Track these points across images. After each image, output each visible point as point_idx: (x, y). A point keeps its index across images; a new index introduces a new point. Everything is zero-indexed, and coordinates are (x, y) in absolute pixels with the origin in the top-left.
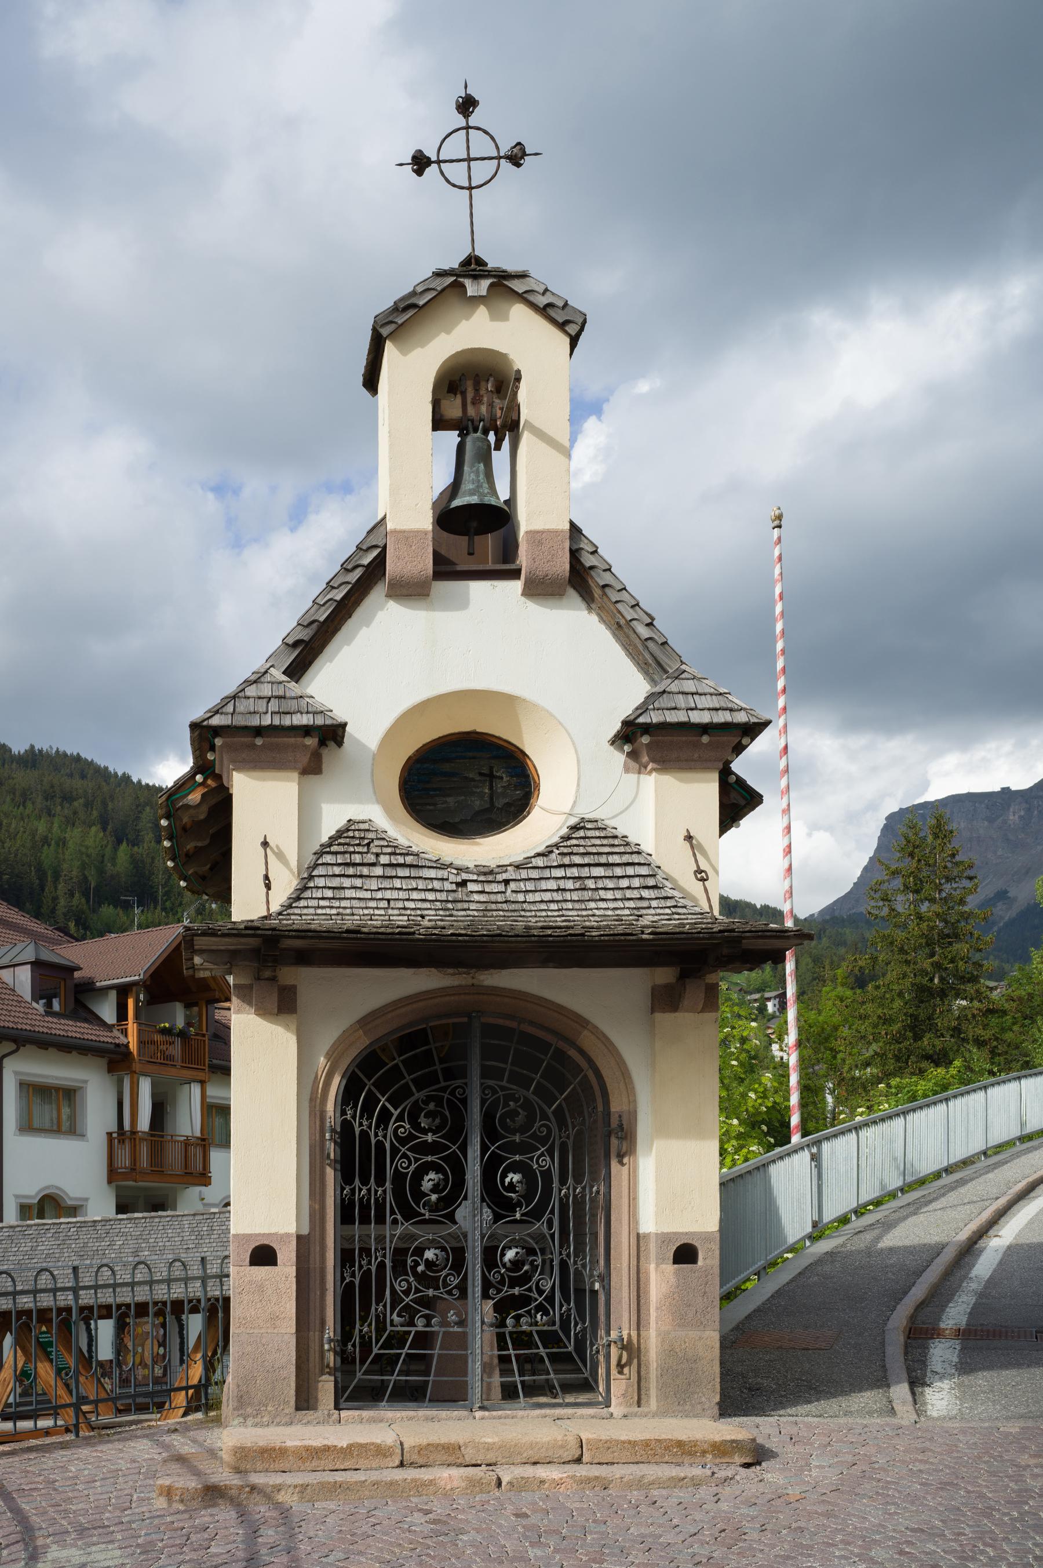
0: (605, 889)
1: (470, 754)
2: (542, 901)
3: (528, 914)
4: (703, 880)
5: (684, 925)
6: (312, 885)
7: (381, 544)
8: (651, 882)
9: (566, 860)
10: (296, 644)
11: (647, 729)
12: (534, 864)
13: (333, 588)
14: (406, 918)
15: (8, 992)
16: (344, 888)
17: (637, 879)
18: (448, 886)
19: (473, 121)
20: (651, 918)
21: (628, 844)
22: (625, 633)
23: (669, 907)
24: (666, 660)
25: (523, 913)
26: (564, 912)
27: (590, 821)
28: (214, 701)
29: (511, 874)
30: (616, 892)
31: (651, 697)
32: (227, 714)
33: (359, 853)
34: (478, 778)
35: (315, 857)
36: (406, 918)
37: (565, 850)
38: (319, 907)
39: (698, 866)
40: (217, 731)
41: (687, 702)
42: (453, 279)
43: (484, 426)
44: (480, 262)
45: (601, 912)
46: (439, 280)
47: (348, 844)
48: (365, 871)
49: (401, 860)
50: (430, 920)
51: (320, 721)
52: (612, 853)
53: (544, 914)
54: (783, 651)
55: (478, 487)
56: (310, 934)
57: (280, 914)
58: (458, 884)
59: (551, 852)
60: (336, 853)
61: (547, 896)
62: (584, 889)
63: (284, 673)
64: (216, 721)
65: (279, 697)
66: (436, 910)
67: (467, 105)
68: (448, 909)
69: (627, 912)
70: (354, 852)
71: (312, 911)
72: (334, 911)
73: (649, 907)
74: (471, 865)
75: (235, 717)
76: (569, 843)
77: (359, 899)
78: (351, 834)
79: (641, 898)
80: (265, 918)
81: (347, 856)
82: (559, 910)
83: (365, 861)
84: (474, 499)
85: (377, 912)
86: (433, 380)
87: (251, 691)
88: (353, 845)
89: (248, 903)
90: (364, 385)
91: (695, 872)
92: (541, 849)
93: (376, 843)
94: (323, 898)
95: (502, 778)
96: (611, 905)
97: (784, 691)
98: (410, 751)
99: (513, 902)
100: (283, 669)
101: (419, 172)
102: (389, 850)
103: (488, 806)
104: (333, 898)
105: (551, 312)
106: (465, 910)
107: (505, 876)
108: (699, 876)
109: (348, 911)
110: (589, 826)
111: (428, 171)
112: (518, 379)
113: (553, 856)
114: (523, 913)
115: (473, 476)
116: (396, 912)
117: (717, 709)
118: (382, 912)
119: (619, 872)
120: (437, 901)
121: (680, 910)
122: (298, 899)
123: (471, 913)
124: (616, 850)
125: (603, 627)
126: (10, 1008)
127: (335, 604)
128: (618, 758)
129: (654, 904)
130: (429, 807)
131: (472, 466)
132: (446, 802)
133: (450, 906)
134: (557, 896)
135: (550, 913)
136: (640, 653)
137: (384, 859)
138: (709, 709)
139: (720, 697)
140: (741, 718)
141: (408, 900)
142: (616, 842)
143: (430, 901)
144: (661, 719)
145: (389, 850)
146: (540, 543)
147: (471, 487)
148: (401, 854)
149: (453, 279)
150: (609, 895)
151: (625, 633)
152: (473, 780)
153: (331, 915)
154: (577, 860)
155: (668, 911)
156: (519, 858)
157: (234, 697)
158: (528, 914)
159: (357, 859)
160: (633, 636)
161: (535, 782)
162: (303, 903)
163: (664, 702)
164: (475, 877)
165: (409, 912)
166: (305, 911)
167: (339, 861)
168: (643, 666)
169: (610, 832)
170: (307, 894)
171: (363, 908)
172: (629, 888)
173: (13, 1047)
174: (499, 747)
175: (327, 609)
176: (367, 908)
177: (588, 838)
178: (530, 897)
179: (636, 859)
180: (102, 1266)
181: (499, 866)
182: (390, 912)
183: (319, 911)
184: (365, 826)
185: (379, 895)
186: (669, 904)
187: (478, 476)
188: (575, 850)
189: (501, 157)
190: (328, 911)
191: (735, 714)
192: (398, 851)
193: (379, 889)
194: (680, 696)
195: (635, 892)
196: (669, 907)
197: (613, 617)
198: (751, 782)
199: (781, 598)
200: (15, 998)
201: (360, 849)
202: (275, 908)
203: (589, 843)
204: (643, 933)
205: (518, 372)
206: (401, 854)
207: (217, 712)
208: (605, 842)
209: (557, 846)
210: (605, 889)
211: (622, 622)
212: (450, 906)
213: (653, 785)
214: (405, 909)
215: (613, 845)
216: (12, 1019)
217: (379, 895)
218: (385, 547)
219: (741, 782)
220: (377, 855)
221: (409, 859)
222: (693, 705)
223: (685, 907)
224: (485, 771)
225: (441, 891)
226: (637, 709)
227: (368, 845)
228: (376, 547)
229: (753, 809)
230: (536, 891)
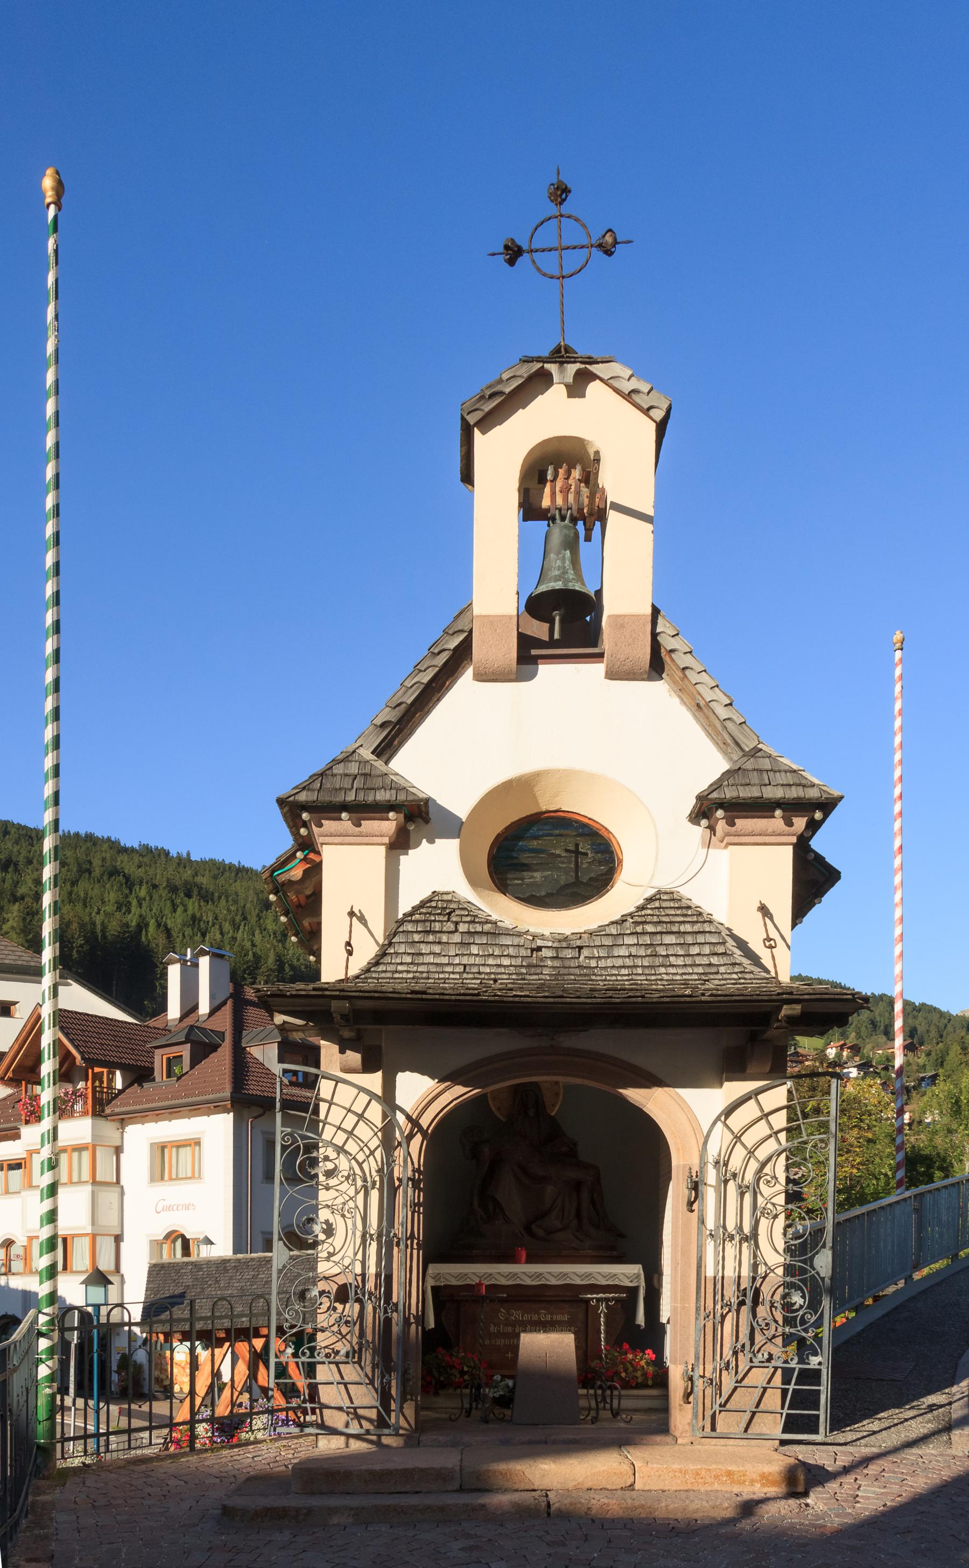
0: (676, 955)
1: (557, 832)
2: (613, 967)
3: (598, 978)
4: (771, 947)
5: (747, 988)
6: (392, 951)
7: (467, 628)
8: (721, 949)
9: (639, 929)
10: (383, 725)
11: (721, 805)
12: (608, 932)
13: (421, 671)
14: (479, 981)
15: (258, 1066)
16: (422, 954)
17: (707, 946)
18: (523, 952)
19: (566, 208)
20: (716, 982)
21: (700, 914)
22: (704, 714)
23: (736, 973)
24: (744, 740)
25: (594, 977)
26: (634, 977)
27: (666, 893)
28: (303, 777)
29: (585, 941)
30: (686, 958)
31: (727, 774)
32: (313, 790)
33: (439, 921)
34: (564, 854)
35: (395, 925)
36: (479, 981)
37: (639, 920)
38: (396, 972)
39: (768, 935)
40: (305, 807)
41: (762, 779)
42: (540, 365)
43: (571, 515)
44: (568, 349)
45: (670, 977)
46: (526, 366)
47: (430, 914)
48: (444, 938)
49: (479, 928)
50: (501, 984)
51: (402, 797)
52: (684, 922)
53: (614, 978)
54: (901, 762)
55: (563, 573)
56: (376, 995)
57: (357, 977)
58: (532, 950)
59: (626, 920)
60: (417, 921)
61: (619, 962)
62: (655, 955)
63: (373, 753)
64: (303, 797)
65: (365, 775)
66: (510, 974)
67: (560, 193)
68: (522, 974)
69: (696, 977)
70: (435, 921)
71: (389, 975)
72: (411, 975)
73: (717, 973)
74: (547, 933)
75: (321, 793)
76: (643, 913)
77: (437, 964)
78: (434, 904)
79: (710, 965)
80: (342, 980)
81: (428, 924)
82: (628, 975)
83: (445, 929)
84: (559, 585)
85: (452, 976)
86: (519, 468)
87: (339, 769)
88: (435, 914)
89: (333, 968)
90: (462, 481)
91: (764, 940)
92: (617, 917)
93: (457, 912)
94: (401, 964)
95: (586, 854)
96: (680, 971)
97: (901, 797)
98: (499, 828)
99: (585, 967)
100: (372, 749)
101: (511, 262)
102: (468, 919)
103: (573, 880)
104: (412, 963)
105: (635, 397)
106: (538, 974)
107: (579, 943)
108: (767, 944)
109: (425, 975)
110: (665, 897)
111: (520, 260)
112: (597, 460)
113: (627, 924)
114: (594, 977)
115: (559, 563)
116: (471, 976)
117: (790, 785)
118: (458, 976)
119: (689, 939)
120: (511, 966)
121: (747, 976)
122: (377, 964)
123: (543, 977)
124: (689, 919)
125: (684, 709)
126: (258, 1079)
127: (423, 686)
128: (698, 832)
129: (722, 969)
130: (516, 882)
131: (558, 553)
132: (532, 877)
133: (524, 971)
134: (628, 962)
135: (619, 978)
136: (718, 733)
137: (462, 928)
138: (782, 785)
139: (794, 774)
140: (813, 794)
141: (484, 965)
142: (690, 912)
143: (505, 966)
144: (735, 794)
145: (468, 919)
146: (622, 626)
147: (557, 573)
148: (479, 923)
149: (540, 365)
150: (680, 961)
151: (704, 714)
152: (559, 856)
153: (407, 979)
154: (650, 928)
155: (735, 976)
156: (593, 926)
157: (322, 774)
158: (598, 978)
159: (437, 926)
160: (712, 717)
161: (618, 859)
162: (381, 968)
163: (740, 779)
164: (550, 944)
165: (483, 976)
166: (383, 975)
167: (419, 929)
168: (722, 745)
169: (684, 903)
170: (387, 959)
171: (439, 973)
172: (698, 955)
173: (260, 1111)
174: (584, 826)
175: (415, 691)
176: (443, 972)
177: (663, 908)
178: (602, 963)
179: (707, 927)
180: (220, 1299)
181: (573, 934)
182: (465, 975)
183: (397, 975)
184: (449, 897)
185: (457, 961)
186: (736, 970)
187: (564, 562)
188: (649, 919)
189: (592, 246)
190: (405, 975)
191: (807, 790)
192: (477, 920)
193: (457, 955)
194: (755, 773)
195: (705, 958)
196: (736, 973)
197: (693, 699)
198: (830, 860)
199: (900, 714)
200: (264, 1071)
201: (441, 918)
202: (354, 971)
203: (667, 913)
204: (703, 995)
205: (597, 453)
206: (479, 923)
207: (304, 788)
208: (679, 912)
209: (631, 915)
210: (676, 955)
211: (702, 703)
212: (524, 971)
213: (724, 858)
214: (479, 973)
215: (686, 915)
216: (259, 1088)
217: (457, 961)
218: (471, 632)
219: (819, 859)
220: (457, 923)
221: (487, 927)
222: (767, 782)
223: (752, 972)
224: (572, 848)
225: (516, 957)
226: (711, 785)
227: (449, 914)
228: (462, 631)
229: (833, 885)
230: (608, 957)
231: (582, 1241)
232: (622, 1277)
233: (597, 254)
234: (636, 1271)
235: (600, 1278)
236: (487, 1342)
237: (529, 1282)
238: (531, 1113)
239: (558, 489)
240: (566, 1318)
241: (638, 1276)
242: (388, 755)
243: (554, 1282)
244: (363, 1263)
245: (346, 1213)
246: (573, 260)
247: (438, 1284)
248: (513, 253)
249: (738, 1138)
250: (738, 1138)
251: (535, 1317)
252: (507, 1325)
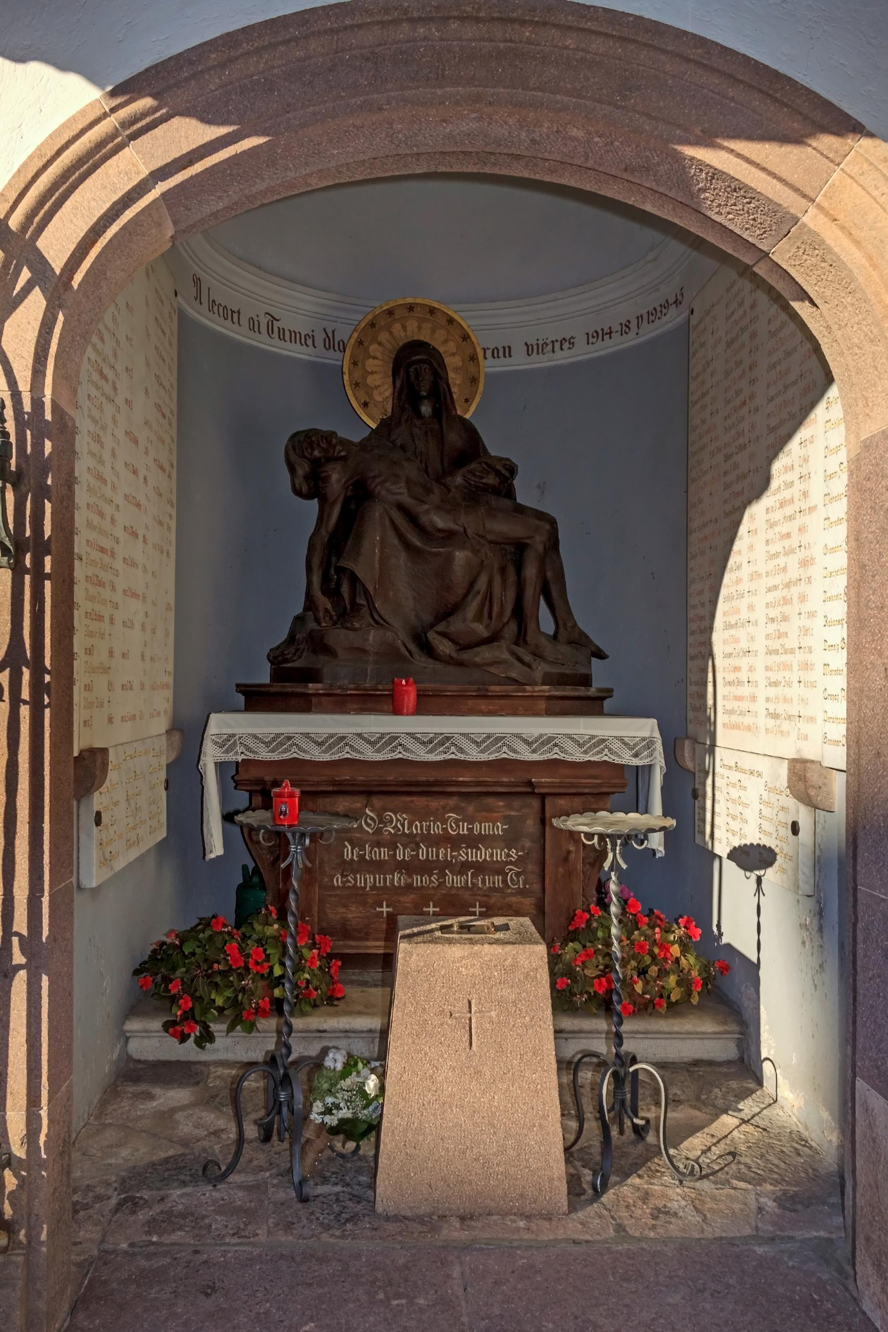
231: (529, 666)
232: (616, 746)
234: (646, 734)
235: (569, 745)
236: (338, 881)
237: (423, 755)
238: (426, 409)
240: (500, 829)
241: (649, 744)
243: (474, 755)
247: (231, 757)
251: (436, 829)
252: (379, 844)
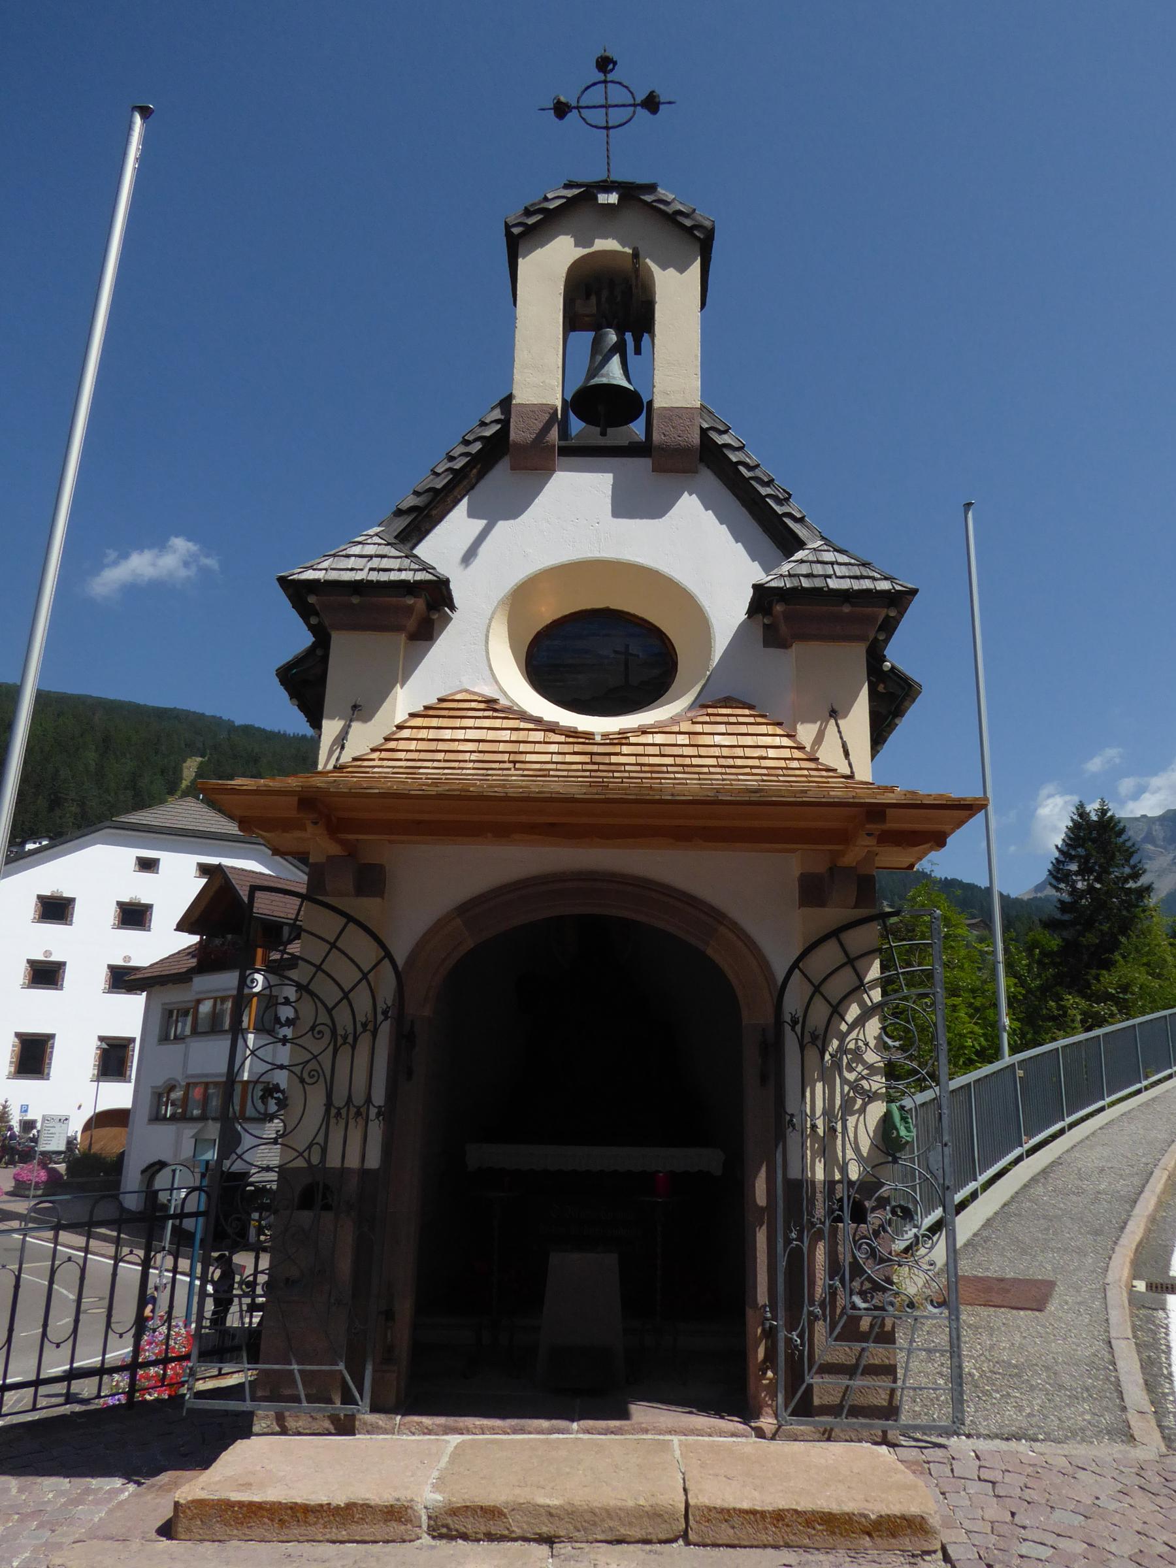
34: (612, 655)
67: (605, 64)
233: (642, 113)
239: (603, 299)
242: (414, 541)
244: (324, 1150)
245: (305, 1075)
246: (617, 116)
248: (561, 110)
249: (817, 989)
250: (817, 989)
